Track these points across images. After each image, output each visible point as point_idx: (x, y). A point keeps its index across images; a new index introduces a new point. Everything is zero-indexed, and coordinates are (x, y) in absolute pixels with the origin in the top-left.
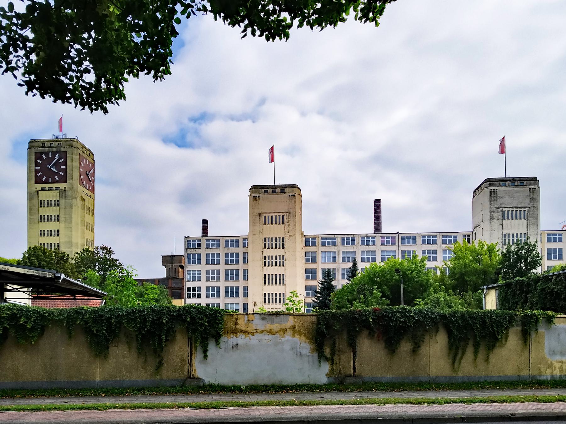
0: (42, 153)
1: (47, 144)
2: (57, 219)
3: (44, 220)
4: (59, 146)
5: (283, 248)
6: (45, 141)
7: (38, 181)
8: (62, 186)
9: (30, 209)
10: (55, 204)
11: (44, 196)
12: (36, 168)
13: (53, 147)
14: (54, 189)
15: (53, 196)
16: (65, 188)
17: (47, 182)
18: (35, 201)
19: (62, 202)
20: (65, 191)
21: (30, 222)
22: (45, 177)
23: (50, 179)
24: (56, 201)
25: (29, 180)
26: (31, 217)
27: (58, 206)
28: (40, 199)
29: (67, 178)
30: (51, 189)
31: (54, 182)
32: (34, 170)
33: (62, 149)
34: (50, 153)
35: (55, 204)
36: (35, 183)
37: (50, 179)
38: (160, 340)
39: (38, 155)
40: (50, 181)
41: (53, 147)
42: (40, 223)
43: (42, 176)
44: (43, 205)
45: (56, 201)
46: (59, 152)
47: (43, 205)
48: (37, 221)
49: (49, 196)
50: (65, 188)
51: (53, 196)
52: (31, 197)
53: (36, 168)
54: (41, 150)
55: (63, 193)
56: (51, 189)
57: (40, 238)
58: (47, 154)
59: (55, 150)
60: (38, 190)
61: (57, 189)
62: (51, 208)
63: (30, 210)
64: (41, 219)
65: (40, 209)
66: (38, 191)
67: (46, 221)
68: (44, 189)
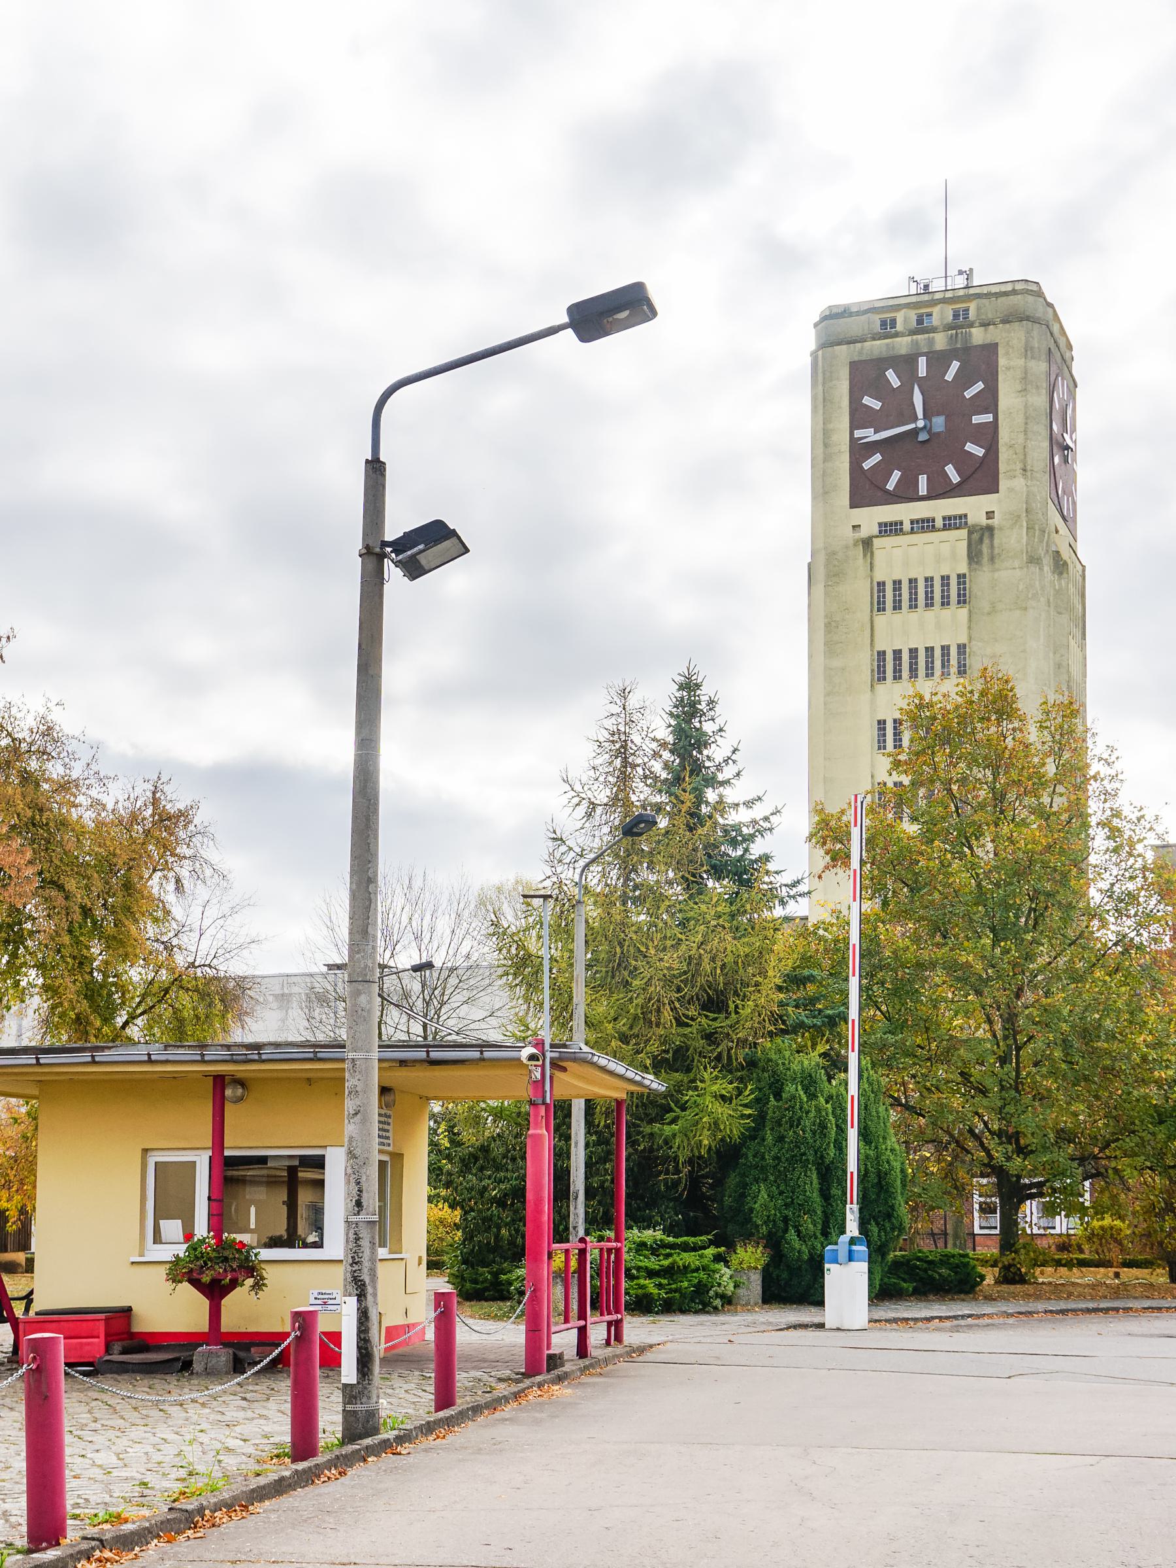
0: (882, 363)
1: (904, 320)
4: (960, 321)
6: (897, 308)
7: (866, 490)
8: (974, 507)
11: (900, 559)
12: (989, 418)
13: (933, 330)
14: (939, 523)
15: (944, 554)
16: (990, 515)
17: (905, 493)
19: (982, 581)
22: (896, 475)
23: (923, 480)
24: (954, 582)
25: (821, 492)
27: (962, 600)
29: (1002, 467)
30: (925, 525)
32: (845, 447)
33: (978, 336)
34: (922, 362)
36: (854, 505)
37: (923, 480)
38: (513, 1309)
39: (866, 377)
40: (923, 490)
41: (933, 330)
42: (880, 688)
43: (883, 471)
45: (954, 582)
46: (964, 352)
48: (866, 675)
50: (990, 515)
51: (944, 554)
53: (989, 418)
54: (877, 347)
55: (980, 541)
56: (925, 525)
58: (905, 364)
59: (940, 341)
60: (864, 533)
61: (952, 523)
65: (881, 620)
66: (867, 543)
68: (890, 529)
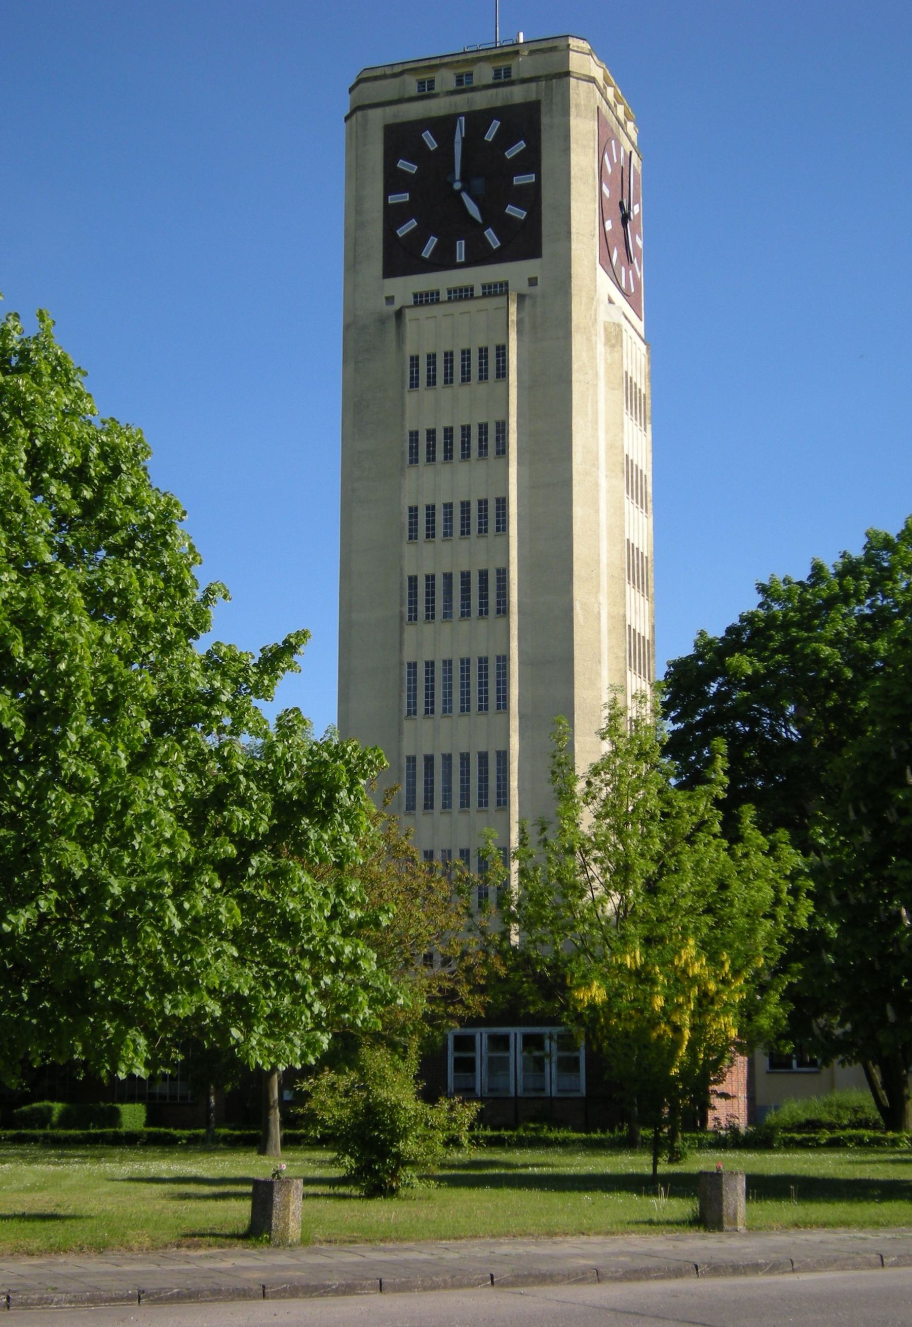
7: (399, 259)
11: (429, 332)
12: (532, 178)
17: (443, 261)
25: (352, 265)
30: (463, 294)
40: (461, 257)
56: (463, 294)
60: (397, 306)
68: (425, 299)
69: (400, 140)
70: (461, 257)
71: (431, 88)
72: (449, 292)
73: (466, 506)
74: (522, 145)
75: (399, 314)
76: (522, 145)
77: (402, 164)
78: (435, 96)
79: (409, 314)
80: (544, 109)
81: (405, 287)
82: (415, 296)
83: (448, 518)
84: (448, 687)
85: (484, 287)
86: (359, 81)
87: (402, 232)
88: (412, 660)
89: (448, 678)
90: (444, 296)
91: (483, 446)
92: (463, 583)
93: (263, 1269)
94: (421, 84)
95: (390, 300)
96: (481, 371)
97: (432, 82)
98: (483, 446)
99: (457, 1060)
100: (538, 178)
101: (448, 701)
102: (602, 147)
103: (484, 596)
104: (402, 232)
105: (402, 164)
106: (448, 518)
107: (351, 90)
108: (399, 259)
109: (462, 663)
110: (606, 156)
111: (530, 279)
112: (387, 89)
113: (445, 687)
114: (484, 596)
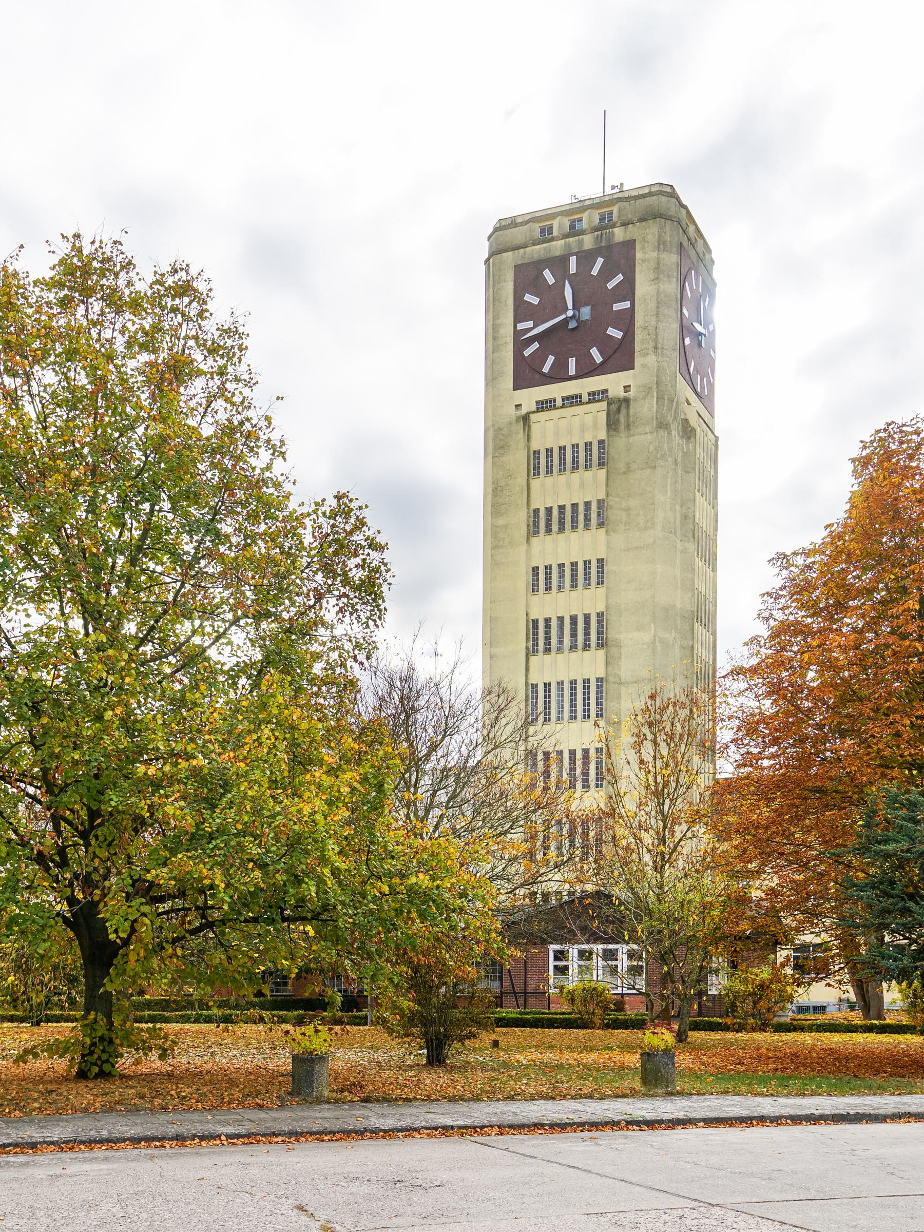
0: (539, 265)
1: (559, 225)
2: (595, 515)
3: (587, 519)
5: (535, 569)
6: (553, 216)
7: (527, 374)
8: (613, 383)
9: (494, 490)
10: (575, 461)
11: (551, 431)
12: (627, 305)
16: (627, 388)
17: (559, 375)
18: (518, 459)
20: (627, 401)
21: (496, 541)
25: (491, 379)
26: (501, 522)
28: (535, 446)
29: (638, 347)
30: (574, 400)
31: (588, 370)
32: (510, 339)
33: (619, 234)
35: (575, 461)
36: (516, 388)
40: (572, 371)
41: (582, 232)
42: (534, 540)
44: (543, 469)
47: (543, 469)
49: (570, 432)
51: (588, 423)
52: (497, 443)
54: (536, 251)
56: (574, 400)
57: (535, 599)
59: (588, 242)
60: (524, 411)
61: (594, 397)
62: (575, 476)
63: (497, 496)
64: (536, 524)
66: (526, 419)
67: (555, 528)
68: (545, 405)
69: (528, 276)
70: (572, 371)
71: (551, 232)
72: (563, 399)
73: (574, 565)
74: (620, 277)
75: (526, 419)
76: (620, 277)
77: (528, 298)
78: (552, 239)
79: (533, 417)
80: (638, 246)
81: (530, 397)
82: (537, 402)
83: (548, 578)
84: (586, 699)
85: (589, 394)
86: (496, 230)
87: (527, 353)
88: (535, 682)
89: (586, 694)
90: (559, 402)
91: (575, 521)
92: (572, 624)
93: (791, 1107)
94: (543, 230)
95: (518, 406)
96: (586, 461)
97: (551, 228)
98: (575, 521)
99: (556, 967)
100: (515, 327)
101: (560, 711)
102: (683, 277)
103: (574, 635)
104: (527, 353)
105: (528, 298)
106: (548, 578)
107: (489, 238)
108: (527, 374)
109: (571, 684)
110: (687, 284)
111: (625, 387)
112: (518, 235)
113: (558, 701)
114: (574, 635)
